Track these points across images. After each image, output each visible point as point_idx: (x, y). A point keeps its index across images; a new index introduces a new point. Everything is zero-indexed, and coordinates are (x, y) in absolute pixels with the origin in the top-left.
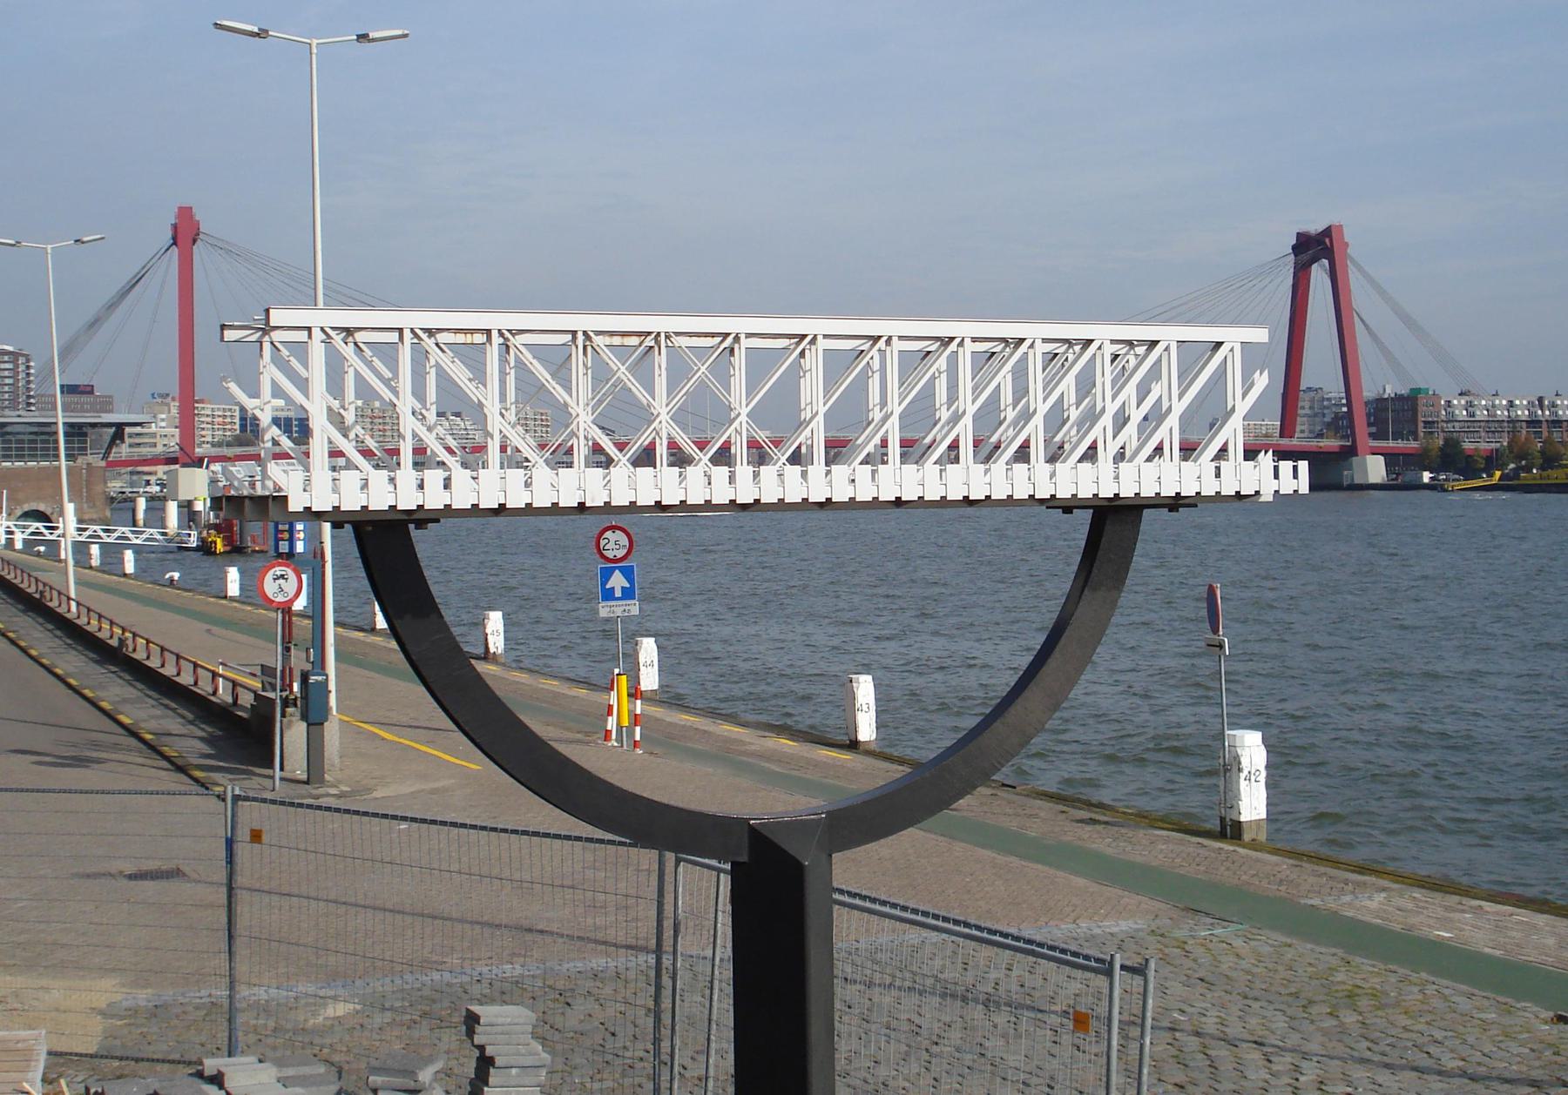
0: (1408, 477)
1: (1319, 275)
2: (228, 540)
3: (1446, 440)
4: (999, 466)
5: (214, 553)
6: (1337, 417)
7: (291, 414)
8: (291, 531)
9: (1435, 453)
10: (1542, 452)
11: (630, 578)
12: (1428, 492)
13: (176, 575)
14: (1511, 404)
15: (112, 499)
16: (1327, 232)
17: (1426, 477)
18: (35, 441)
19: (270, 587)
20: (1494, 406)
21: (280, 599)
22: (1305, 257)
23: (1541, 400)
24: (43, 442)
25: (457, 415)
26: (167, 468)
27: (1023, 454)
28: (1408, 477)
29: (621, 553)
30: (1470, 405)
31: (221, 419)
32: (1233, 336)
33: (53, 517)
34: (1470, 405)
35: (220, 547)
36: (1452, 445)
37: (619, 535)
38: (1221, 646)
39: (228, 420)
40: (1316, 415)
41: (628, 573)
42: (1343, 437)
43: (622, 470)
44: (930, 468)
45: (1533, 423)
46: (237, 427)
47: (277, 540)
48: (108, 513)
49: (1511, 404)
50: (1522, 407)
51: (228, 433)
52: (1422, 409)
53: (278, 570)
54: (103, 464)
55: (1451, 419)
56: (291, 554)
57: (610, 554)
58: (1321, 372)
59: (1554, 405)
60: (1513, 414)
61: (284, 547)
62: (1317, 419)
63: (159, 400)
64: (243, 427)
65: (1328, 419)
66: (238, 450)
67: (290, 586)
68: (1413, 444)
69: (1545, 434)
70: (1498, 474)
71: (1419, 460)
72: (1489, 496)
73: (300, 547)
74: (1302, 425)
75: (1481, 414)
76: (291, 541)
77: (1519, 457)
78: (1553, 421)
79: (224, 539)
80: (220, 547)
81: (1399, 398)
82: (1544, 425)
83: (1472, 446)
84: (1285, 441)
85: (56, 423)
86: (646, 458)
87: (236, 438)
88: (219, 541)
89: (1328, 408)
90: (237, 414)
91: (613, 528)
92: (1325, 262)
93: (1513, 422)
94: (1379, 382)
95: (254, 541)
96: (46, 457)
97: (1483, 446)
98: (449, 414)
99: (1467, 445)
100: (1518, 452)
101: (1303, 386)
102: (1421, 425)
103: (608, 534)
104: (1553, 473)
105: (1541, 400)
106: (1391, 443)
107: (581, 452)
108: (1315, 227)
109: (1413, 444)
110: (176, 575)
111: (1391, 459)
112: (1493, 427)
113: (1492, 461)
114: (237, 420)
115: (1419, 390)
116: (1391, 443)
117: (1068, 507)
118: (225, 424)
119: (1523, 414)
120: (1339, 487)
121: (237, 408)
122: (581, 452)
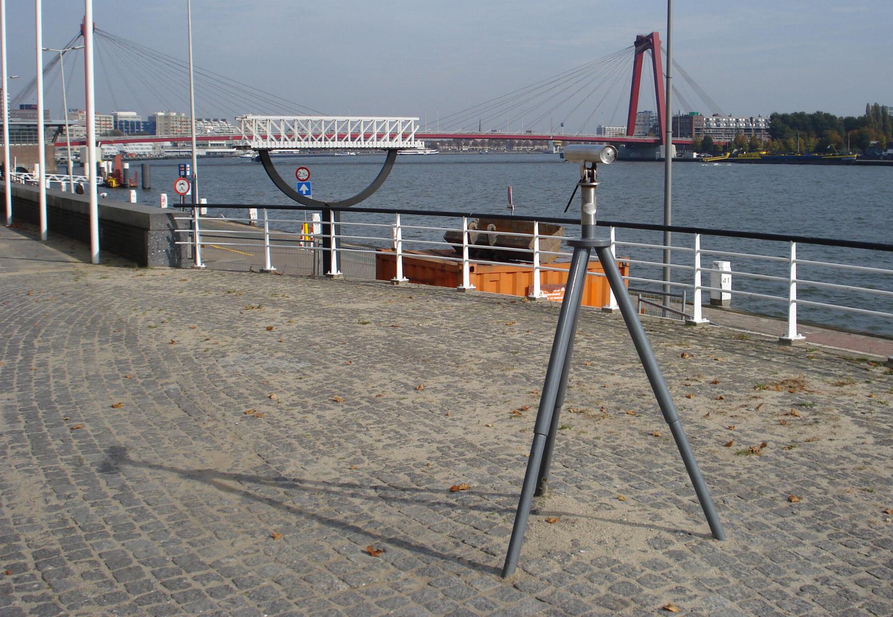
0: (687, 154)
1: (647, 56)
2: (118, 181)
3: (705, 137)
4: (355, 142)
5: (112, 187)
6: (655, 126)
7: (140, 120)
8: (185, 167)
9: (699, 144)
10: (750, 144)
11: (309, 188)
12: (695, 163)
13: (105, 194)
14: (737, 121)
15: (58, 162)
16: (651, 36)
17: (695, 155)
18: (19, 134)
19: (178, 187)
20: (729, 121)
21: (182, 192)
22: (640, 48)
23: (751, 119)
24: (23, 134)
25: (224, 120)
26: (78, 147)
27: (360, 140)
28: (687, 154)
29: (305, 178)
30: (718, 120)
31: (104, 122)
32: (412, 119)
33: (29, 171)
34: (718, 120)
35: (114, 184)
36: (708, 139)
37: (305, 171)
38: (512, 208)
39: (108, 123)
40: (646, 125)
41: (308, 185)
42: (656, 136)
43: (303, 142)
44: (343, 142)
45: (747, 130)
46: (113, 126)
47: (180, 171)
48: (56, 169)
49: (737, 121)
50: (743, 122)
51: (108, 129)
52: (694, 122)
53: (181, 182)
54: (53, 144)
55: (709, 128)
56: (185, 176)
57: (301, 178)
58: (647, 103)
59: (757, 121)
60: (738, 126)
61: (182, 173)
62: (647, 127)
63: (73, 113)
64: (116, 126)
65: (651, 127)
66: (116, 138)
67: (186, 187)
68: (690, 139)
69: (753, 135)
70: (728, 154)
71: (692, 147)
72: (723, 164)
73: (188, 173)
74: (637, 130)
75: (723, 125)
76: (185, 171)
77: (738, 147)
78: (757, 129)
79: (116, 180)
80: (114, 184)
81: (686, 117)
82: (753, 131)
83: (717, 141)
84: (629, 137)
85: (36, 125)
86: (307, 140)
87: (112, 131)
88: (114, 181)
89: (652, 121)
90: (112, 120)
91: (302, 168)
92: (650, 50)
93: (738, 129)
94: (676, 109)
95: (130, 182)
96: (30, 141)
97: (722, 141)
98: (212, 120)
99: (715, 140)
100: (739, 144)
101: (638, 111)
102: (694, 130)
103: (300, 170)
104: (753, 154)
105: (751, 119)
106: (679, 139)
107: (296, 139)
108: (645, 33)
109: (690, 139)
110: (105, 194)
111: (679, 146)
112: (728, 131)
113: (726, 148)
114: (112, 123)
115: (693, 113)
116: (679, 139)
117: (384, 149)
118: (106, 124)
119: (743, 125)
120: (653, 160)
121: (112, 117)
122: (296, 139)
